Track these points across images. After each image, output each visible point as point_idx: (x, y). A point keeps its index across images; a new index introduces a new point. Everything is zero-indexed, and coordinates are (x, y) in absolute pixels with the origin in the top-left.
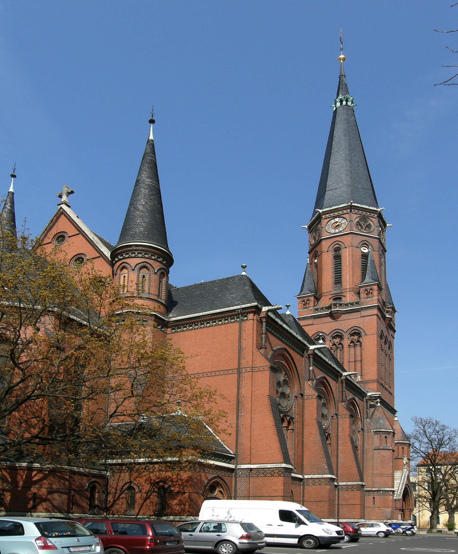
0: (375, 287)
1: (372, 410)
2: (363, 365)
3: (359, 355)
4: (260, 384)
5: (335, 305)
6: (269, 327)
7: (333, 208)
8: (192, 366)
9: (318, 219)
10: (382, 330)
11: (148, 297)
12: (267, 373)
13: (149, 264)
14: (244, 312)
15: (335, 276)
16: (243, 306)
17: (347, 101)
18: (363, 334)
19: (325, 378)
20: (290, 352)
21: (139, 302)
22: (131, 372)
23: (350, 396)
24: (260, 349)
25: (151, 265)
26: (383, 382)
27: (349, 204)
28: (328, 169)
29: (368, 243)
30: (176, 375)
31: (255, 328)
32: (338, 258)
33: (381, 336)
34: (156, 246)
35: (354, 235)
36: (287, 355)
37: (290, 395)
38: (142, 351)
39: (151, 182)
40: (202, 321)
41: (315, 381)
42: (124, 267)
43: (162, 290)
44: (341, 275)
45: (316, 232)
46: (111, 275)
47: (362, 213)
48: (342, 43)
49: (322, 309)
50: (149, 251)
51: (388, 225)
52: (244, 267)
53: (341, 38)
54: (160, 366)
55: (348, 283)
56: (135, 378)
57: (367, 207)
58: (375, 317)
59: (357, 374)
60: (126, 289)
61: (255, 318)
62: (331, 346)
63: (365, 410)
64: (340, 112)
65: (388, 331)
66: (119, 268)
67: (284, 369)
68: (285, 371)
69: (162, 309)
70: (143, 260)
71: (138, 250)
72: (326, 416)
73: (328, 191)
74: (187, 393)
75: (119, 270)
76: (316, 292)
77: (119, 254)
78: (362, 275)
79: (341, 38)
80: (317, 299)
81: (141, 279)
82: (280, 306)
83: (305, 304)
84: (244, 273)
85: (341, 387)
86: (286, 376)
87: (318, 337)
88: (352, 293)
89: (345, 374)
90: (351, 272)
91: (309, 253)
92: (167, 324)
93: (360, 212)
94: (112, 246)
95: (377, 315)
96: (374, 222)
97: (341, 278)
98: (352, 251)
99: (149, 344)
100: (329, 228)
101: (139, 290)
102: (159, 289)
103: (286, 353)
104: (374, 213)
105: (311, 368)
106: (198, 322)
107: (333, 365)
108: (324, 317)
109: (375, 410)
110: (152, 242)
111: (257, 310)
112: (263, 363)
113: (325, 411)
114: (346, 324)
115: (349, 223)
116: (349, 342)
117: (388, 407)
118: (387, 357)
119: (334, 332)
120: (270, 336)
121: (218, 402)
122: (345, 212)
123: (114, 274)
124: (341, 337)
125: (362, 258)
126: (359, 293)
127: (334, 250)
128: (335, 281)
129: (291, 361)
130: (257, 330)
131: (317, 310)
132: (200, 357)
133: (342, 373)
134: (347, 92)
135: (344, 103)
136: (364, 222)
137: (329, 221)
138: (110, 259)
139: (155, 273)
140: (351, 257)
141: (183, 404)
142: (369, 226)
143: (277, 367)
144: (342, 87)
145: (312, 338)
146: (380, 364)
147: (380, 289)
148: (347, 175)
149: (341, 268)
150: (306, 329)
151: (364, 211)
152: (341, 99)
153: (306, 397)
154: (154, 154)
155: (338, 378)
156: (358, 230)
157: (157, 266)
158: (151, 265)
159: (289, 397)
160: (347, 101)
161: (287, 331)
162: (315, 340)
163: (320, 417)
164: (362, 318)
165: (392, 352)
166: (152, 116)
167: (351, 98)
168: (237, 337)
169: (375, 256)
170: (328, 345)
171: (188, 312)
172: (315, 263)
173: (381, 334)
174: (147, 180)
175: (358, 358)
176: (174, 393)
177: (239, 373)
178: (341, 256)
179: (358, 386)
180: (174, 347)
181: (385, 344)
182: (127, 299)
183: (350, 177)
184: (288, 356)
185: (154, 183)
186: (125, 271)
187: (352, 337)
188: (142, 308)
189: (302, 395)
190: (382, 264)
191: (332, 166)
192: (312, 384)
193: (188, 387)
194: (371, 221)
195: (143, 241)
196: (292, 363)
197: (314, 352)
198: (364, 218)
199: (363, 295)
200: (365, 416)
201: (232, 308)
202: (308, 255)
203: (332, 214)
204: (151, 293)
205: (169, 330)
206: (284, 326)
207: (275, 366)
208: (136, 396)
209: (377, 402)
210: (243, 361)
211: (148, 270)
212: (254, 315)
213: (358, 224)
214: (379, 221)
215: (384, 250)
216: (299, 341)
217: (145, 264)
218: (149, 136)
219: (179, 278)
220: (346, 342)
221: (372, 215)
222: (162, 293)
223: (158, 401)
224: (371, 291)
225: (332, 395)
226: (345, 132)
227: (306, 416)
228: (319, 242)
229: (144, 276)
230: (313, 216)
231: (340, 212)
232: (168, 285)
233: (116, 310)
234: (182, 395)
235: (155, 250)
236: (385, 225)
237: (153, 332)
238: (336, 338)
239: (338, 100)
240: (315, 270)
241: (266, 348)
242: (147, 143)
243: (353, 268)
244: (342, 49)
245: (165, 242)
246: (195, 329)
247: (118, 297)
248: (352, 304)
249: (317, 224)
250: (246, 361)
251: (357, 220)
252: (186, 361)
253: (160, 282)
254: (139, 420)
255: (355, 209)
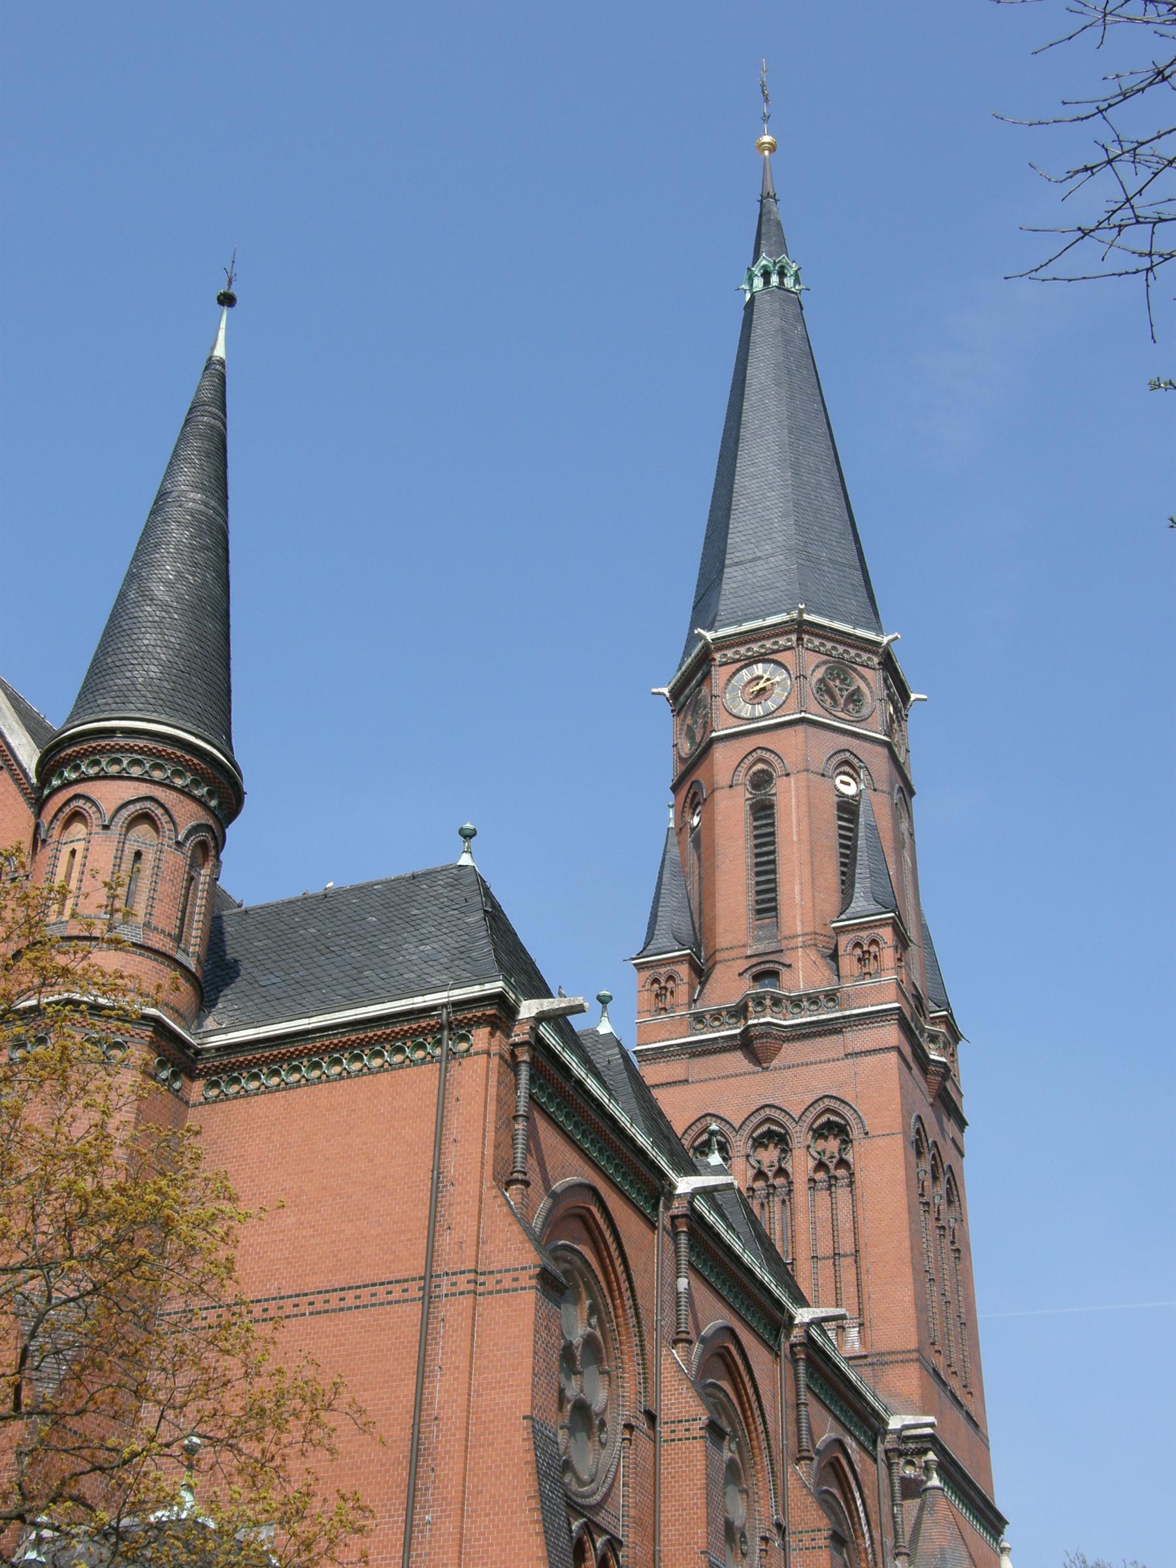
0: (887, 934)
1: (912, 1505)
2: (864, 1277)
3: (849, 1225)
4: (502, 1345)
5: (759, 1000)
6: (541, 1087)
7: (747, 626)
8: (266, 1254)
9: (700, 666)
10: (919, 1118)
11: (140, 941)
12: (528, 1299)
13: (162, 806)
14: (458, 1021)
15: (758, 883)
16: (459, 994)
17: (782, 274)
18: (855, 1133)
19: (731, 1331)
20: (610, 1205)
21: (107, 960)
22: (29, 1286)
23: (827, 1431)
24: (509, 1183)
25: (167, 811)
26: (939, 1362)
27: (795, 615)
28: (731, 491)
29: (855, 761)
30: (196, 1303)
31: (493, 1091)
32: (763, 810)
33: (919, 1145)
34: (209, 748)
35: (811, 730)
36: (598, 1216)
37: (608, 1417)
38: (87, 1184)
39: (206, 505)
40: (317, 1053)
41: (697, 1347)
42: (77, 816)
43: (192, 913)
44: (774, 881)
45: (695, 713)
46: (27, 845)
47: (834, 648)
48: (766, 100)
49: (716, 1015)
50: (169, 758)
51: (913, 696)
52: (468, 835)
53: (763, 85)
54: (142, 1258)
55: (798, 912)
56: (41, 1318)
57: (848, 628)
58: (893, 1056)
59: (843, 1317)
60: (69, 903)
61: (495, 1049)
62: (750, 1183)
63: (886, 1508)
64: (764, 307)
65: (940, 1123)
66: (62, 816)
67: (587, 1286)
68: (591, 1295)
69: (185, 995)
70: (144, 789)
71: (131, 750)
72: (743, 1535)
73: (730, 566)
74: (227, 1396)
75: (58, 825)
76: (697, 945)
77: (65, 763)
78: (843, 882)
79: (763, 85)
80: (701, 973)
81: (126, 865)
82: (579, 1000)
83: (661, 991)
84: (465, 860)
85: (790, 1383)
86: (594, 1321)
87: (705, 1137)
88: (814, 955)
89: (803, 1315)
90: (807, 869)
91: (675, 788)
92: (194, 1062)
93: (829, 645)
94: (48, 729)
95: (898, 1049)
96: (871, 682)
97: (774, 890)
98: (808, 787)
99: (119, 1154)
100: (734, 698)
101: (113, 911)
102: (185, 909)
103: (594, 1209)
104: (869, 651)
105: (683, 1283)
106: (300, 1056)
107: (757, 1271)
108: (724, 1050)
109: (921, 1509)
110: (180, 723)
111: (501, 1012)
112: (515, 1254)
113: (738, 1512)
114: (799, 1081)
115: (796, 684)
116: (811, 1164)
117: (968, 1496)
118: (947, 1241)
119: (756, 1120)
120: (544, 1130)
121: (340, 1447)
122: (782, 641)
123: (38, 842)
124: (781, 1140)
125: (840, 818)
126: (834, 956)
127: (751, 782)
128: (757, 902)
129: (613, 1247)
130: (499, 1100)
131: (699, 1018)
132: (291, 1220)
133: (672, 1174)
134: (782, 247)
135: (775, 280)
136: (843, 681)
137: (735, 674)
138: (34, 780)
139: (178, 843)
140: (804, 809)
141: (207, 1456)
142: (855, 698)
143: (565, 1272)
144: (767, 231)
145: (686, 1143)
146: (925, 1277)
147: (902, 942)
148: (785, 515)
149: (773, 852)
150: (665, 1099)
151: (841, 643)
152: (764, 267)
153: (664, 1431)
154: (223, 407)
155: (777, 1337)
156: (823, 712)
157: (188, 814)
158: (167, 811)
159: (603, 1424)
160: (782, 274)
161: (600, 1106)
162: (696, 1149)
163: (720, 1542)
164: (850, 1061)
165: (961, 1220)
166: (230, 282)
167: (794, 267)
168: (429, 1128)
169: (877, 811)
170: (739, 1177)
171: (271, 1012)
172: (693, 829)
173: (918, 1132)
174: (191, 496)
175: (847, 1246)
176: (179, 1398)
177: (428, 1299)
178: (772, 807)
179: (853, 1378)
180: (206, 1170)
181: (935, 1178)
182: (65, 945)
183: (797, 523)
184: (601, 1221)
185: (213, 508)
186: (78, 829)
187: (821, 1144)
188: (115, 988)
189: (651, 1417)
190: (905, 842)
191: (743, 482)
192: (688, 1363)
193: (232, 1366)
194: (862, 677)
195: (154, 716)
196: (604, 1227)
197: (693, 1209)
198: (840, 670)
199: (848, 964)
200: (889, 1542)
201: (419, 1002)
202: (670, 798)
203: (742, 650)
204: (154, 923)
205: (197, 1090)
206: (592, 1084)
207: (556, 1269)
208: (30, 1414)
209: (927, 1469)
210: (446, 1241)
211: (157, 830)
212: (492, 1034)
213: (824, 688)
214: (885, 680)
215: (907, 790)
216: (641, 1152)
217: (148, 804)
218: (213, 348)
219: (262, 866)
220: (801, 1165)
221: (865, 656)
222: (190, 927)
223: (111, 1442)
224: (874, 949)
225: (759, 1421)
226: (775, 370)
227: (669, 1533)
228: (705, 750)
229: (138, 855)
230: (687, 653)
231: (768, 644)
232: (215, 895)
233: (20, 994)
234: (209, 1406)
235: (188, 752)
236: (905, 697)
237: (141, 1098)
238: (766, 1147)
239: (757, 270)
240: (693, 858)
241: (527, 1184)
242: (207, 368)
243: (812, 853)
244: (766, 118)
245: (222, 729)
246: (288, 1087)
247: (38, 938)
248: (814, 1000)
249: (700, 684)
250: (455, 1250)
251: (820, 673)
252: (240, 1231)
253: (191, 879)
254: (20, 1551)
255: (812, 634)
